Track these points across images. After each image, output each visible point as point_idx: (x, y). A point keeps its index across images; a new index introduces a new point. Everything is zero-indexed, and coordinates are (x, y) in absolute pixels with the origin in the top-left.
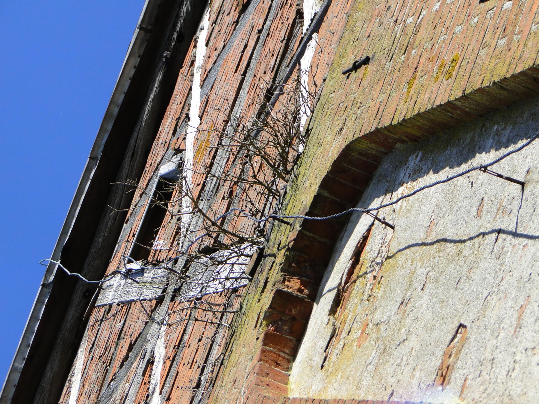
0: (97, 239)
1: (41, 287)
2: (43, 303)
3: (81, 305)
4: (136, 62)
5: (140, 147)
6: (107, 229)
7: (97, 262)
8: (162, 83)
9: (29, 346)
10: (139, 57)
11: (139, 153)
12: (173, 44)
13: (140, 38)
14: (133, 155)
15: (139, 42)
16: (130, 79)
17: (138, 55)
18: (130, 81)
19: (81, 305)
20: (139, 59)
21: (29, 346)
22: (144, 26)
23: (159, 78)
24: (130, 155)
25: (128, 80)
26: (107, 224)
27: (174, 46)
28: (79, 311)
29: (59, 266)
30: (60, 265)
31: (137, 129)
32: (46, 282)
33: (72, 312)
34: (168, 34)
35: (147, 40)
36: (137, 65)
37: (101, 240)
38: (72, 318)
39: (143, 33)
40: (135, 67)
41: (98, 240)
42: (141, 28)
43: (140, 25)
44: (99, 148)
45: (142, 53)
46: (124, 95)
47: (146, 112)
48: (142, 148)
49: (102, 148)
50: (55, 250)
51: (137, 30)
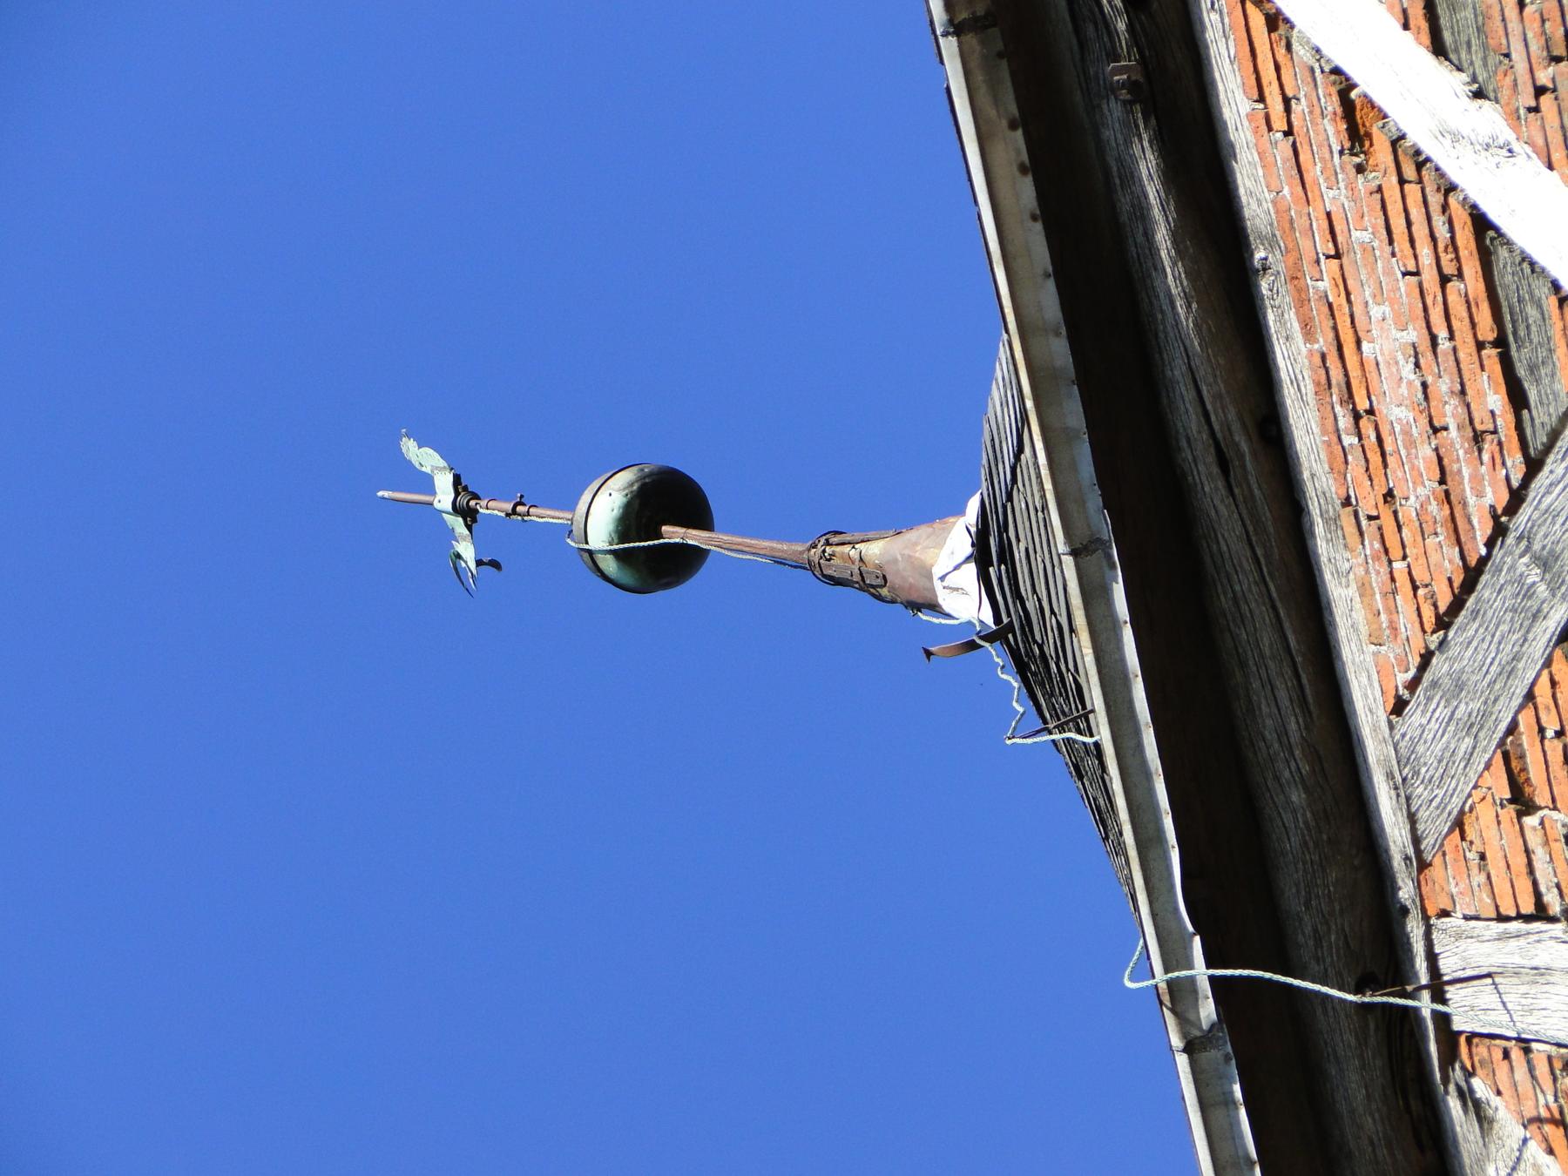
0: (1279, 800)
1: (1182, 1061)
2: (1230, 1102)
3: (1372, 1041)
4: (1018, 152)
5: (1236, 427)
6: (1297, 752)
7: (1333, 875)
8: (1172, 174)
9: (1253, 1163)
10: (1013, 126)
11: (1245, 447)
12: (1121, 26)
13: (974, 63)
14: (1224, 464)
15: (979, 78)
16: (1034, 218)
17: (1004, 123)
18: (1039, 226)
19: (1372, 1041)
20: (1019, 132)
21: (1253, 1163)
22: (963, 15)
23: (1147, 166)
24: (1215, 470)
25: (1030, 224)
26: (1283, 733)
27: (1131, 28)
28: (1379, 1063)
29: (1212, 979)
30: (1211, 972)
31: (1178, 371)
32: (1197, 1033)
33: (1354, 1077)
34: (1419, 948)
35: (1000, 55)
36: (1025, 157)
37: (1297, 797)
38: (1368, 1096)
39: (971, 39)
40: (1023, 170)
41: (1288, 801)
42: (956, 29)
43: (951, 22)
44: (1082, 503)
45: (1013, 109)
46: (1051, 285)
47: (1179, 303)
48: (1244, 426)
49: (1094, 499)
50: (1154, 915)
51: (949, 46)
